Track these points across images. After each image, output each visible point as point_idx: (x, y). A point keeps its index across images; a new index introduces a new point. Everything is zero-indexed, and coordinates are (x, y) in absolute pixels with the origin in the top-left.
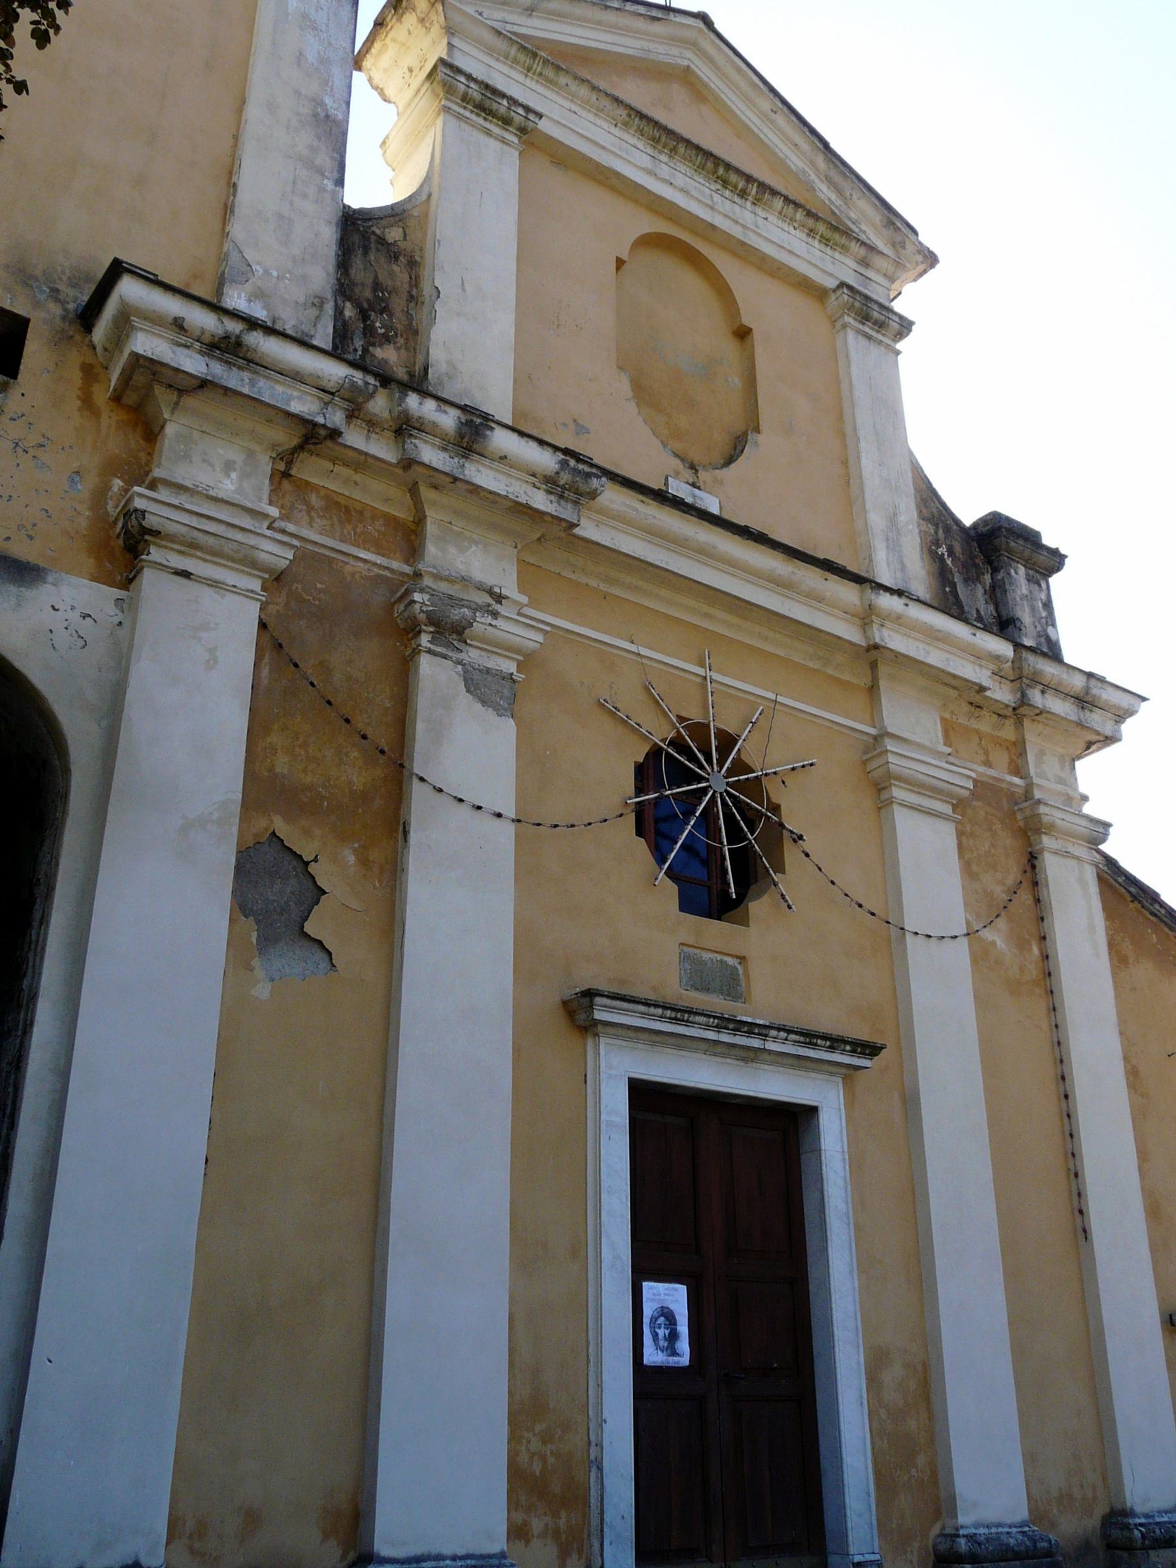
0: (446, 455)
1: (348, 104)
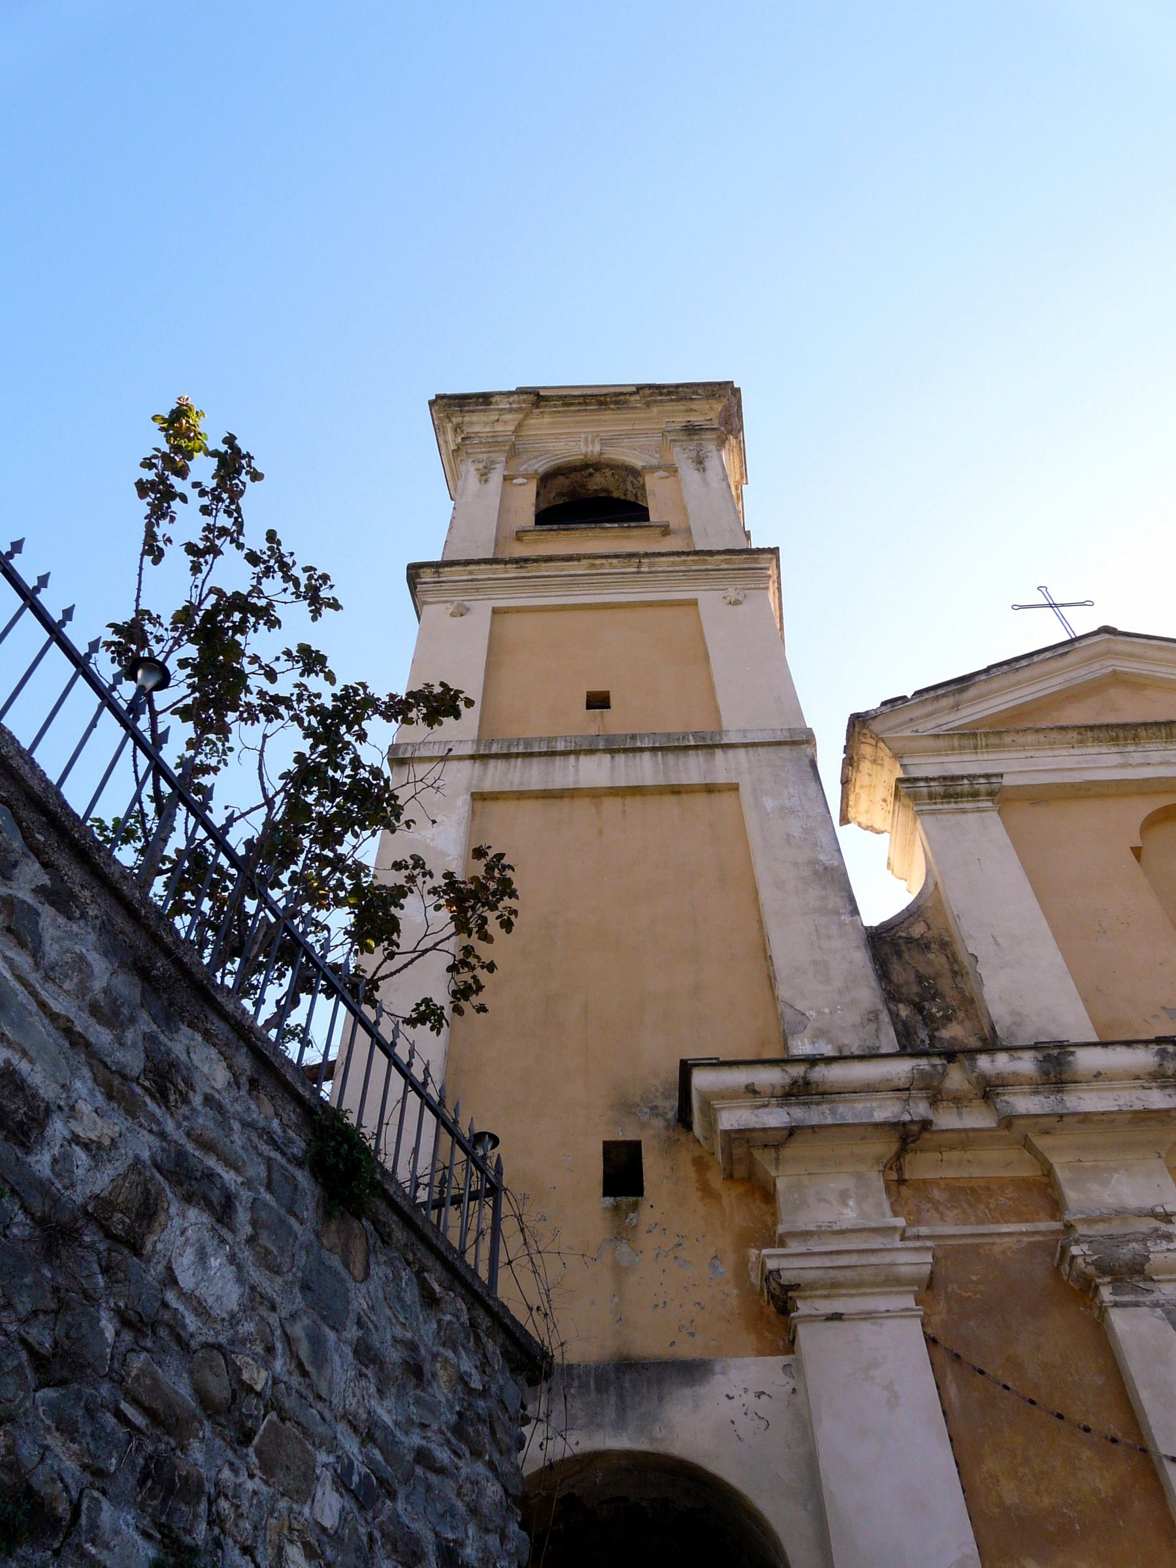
0: (1041, 1098)
1: (839, 850)
